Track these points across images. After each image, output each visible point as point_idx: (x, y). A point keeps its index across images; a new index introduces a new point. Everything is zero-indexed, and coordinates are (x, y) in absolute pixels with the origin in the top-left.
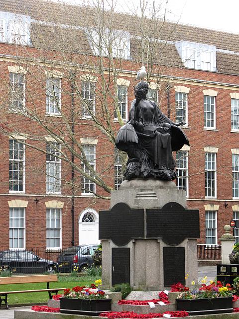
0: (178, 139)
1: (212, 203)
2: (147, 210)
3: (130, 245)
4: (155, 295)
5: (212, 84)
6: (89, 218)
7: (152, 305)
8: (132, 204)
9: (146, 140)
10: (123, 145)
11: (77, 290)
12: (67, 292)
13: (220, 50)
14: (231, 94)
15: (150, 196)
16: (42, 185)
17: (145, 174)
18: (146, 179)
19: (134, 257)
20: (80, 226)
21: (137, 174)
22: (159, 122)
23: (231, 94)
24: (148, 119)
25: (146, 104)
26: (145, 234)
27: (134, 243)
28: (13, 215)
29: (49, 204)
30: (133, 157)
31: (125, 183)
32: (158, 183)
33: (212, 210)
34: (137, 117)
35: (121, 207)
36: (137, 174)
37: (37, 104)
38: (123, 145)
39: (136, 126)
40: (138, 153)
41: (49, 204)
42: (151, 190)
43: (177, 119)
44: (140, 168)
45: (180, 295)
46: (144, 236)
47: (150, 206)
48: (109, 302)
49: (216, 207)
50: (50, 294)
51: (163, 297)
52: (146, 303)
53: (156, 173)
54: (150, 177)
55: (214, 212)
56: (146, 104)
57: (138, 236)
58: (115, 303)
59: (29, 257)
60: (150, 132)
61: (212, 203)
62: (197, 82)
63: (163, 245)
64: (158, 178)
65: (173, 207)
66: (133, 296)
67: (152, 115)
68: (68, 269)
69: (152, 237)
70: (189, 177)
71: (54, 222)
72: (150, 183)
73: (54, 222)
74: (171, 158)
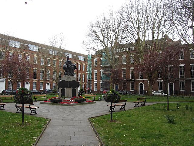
3: (65, 88)
4: (70, 99)
6: (48, 84)
7: (70, 101)
8: (66, 80)
9: (69, 67)
10: (64, 68)
11: (54, 98)
12: (52, 98)
14: (155, 39)
15: (69, 79)
16: (40, 78)
18: (68, 75)
20: (25, 85)
23: (155, 39)
24: (69, 63)
25: (69, 60)
28: (34, 83)
29: (41, 81)
30: (66, 71)
31: (64, 76)
32: (71, 76)
34: (67, 63)
35: (63, 81)
37: (39, 62)
38: (64, 68)
39: (67, 65)
40: (67, 70)
41: (41, 81)
43: (42, 73)
45: (76, 99)
47: (70, 81)
48: (61, 100)
51: (72, 99)
52: (69, 100)
54: (69, 75)
56: (69, 60)
57: (67, 87)
58: (63, 100)
59: (37, 91)
63: (72, 88)
64: (71, 75)
65: (74, 81)
66: (66, 99)
68: (45, 94)
69: (70, 87)
71: (41, 85)
72: (70, 76)
73: (41, 85)
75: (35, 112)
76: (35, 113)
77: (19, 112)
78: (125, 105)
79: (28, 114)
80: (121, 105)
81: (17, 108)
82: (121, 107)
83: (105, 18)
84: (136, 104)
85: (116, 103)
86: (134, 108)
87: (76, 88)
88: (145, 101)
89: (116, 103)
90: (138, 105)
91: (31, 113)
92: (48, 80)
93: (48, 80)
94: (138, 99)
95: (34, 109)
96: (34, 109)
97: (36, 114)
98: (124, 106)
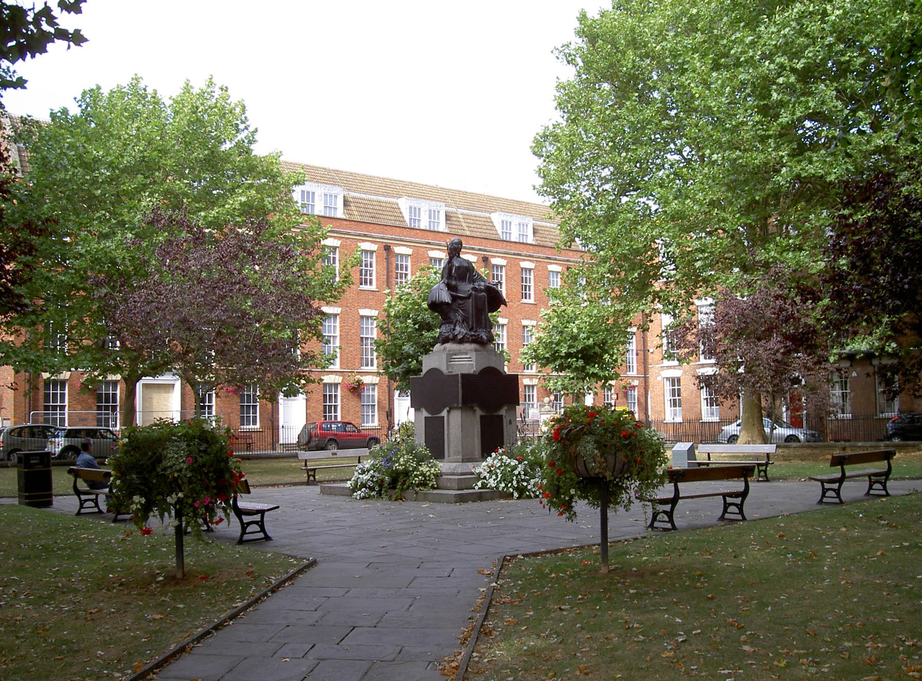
0: (494, 299)
1: (531, 377)
2: (463, 375)
3: (444, 413)
5: (530, 256)
13: (539, 223)
17: (460, 337)
18: (461, 342)
19: (448, 428)
21: (451, 337)
22: (474, 281)
26: (460, 401)
27: (449, 412)
33: (530, 383)
36: (451, 337)
39: (450, 287)
42: (466, 354)
44: (454, 329)
46: (458, 403)
49: (535, 381)
50: (673, 525)
53: (472, 336)
55: (533, 386)
60: (465, 292)
61: (531, 377)
62: (514, 254)
63: (479, 412)
64: (473, 341)
67: (466, 272)
70: (458, 208)
74: (487, 319)
75: (263, 529)
76: (261, 535)
77: (826, 503)
78: (744, 494)
79: (230, 539)
80: (725, 496)
81: (80, 498)
82: (726, 506)
83: (313, 570)
84: (827, 486)
85: (845, 467)
86: (820, 507)
87: (503, 412)
88: (885, 469)
89: (681, 485)
90: (838, 492)
91: (244, 532)
92: (367, 287)
93: (367, 287)
94: (838, 461)
95: (257, 518)
96: (257, 518)
97: (267, 538)
98: (836, 486)
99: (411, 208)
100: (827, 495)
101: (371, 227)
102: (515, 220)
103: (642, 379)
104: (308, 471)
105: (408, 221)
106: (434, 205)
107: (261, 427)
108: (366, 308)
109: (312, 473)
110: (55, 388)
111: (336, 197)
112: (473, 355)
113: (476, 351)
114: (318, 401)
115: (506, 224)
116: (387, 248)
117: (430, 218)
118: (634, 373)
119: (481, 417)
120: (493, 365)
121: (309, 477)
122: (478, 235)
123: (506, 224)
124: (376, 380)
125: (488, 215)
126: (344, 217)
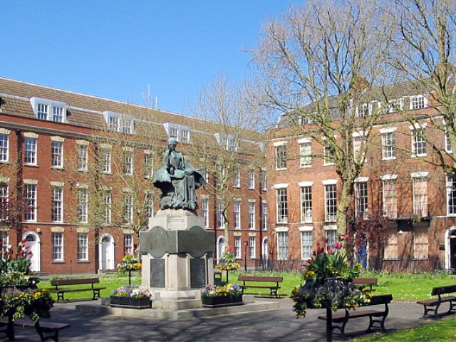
2: (179, 232)
18: (177, 208)
99: (39, 105)
100: (374, 325)
101: (85, 130)
102: (50, 103)
103: (259, 233)
104: (94, 290)
105: (36, 112)
106: (58, 103)
107: (64, 259)
108: (55, 181)
109: (61, 295)
110: (57, 237)
111: (61, 109)
112: (186, 218)
113: (187, 215)
114: (48, 244)
115: (42, 107)
116: (19, 133)
117: (54, 113)
118: (253, 228)
119: (191, 259)
120: (198, 225)
121: (95, 294)
122: (21, 115)
123: (42, 107)
124: (255, 234)
125: (26, 99)
126: (67, 122)
